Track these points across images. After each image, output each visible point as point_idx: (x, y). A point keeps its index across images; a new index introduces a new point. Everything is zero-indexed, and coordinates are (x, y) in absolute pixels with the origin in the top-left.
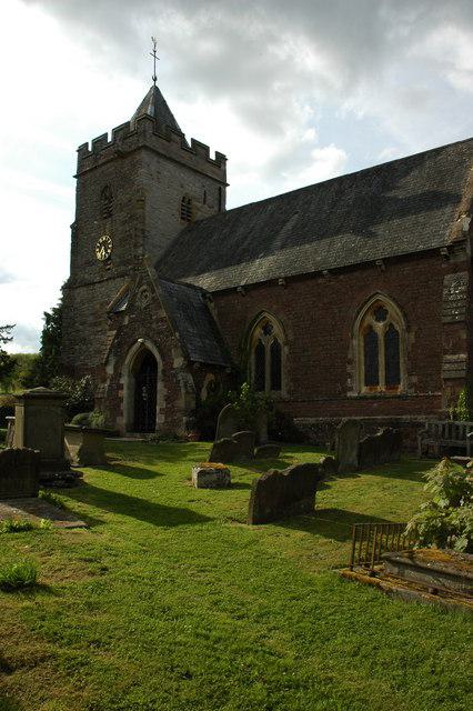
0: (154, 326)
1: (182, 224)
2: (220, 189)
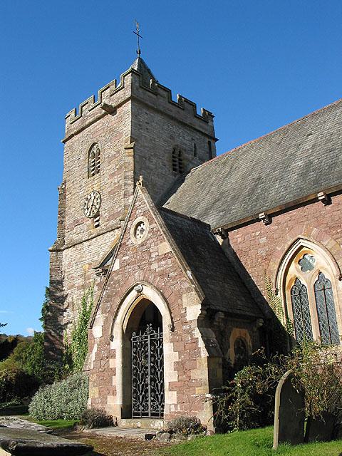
0: (155, 266)
1: (175, 175)
2: (209, 143)
